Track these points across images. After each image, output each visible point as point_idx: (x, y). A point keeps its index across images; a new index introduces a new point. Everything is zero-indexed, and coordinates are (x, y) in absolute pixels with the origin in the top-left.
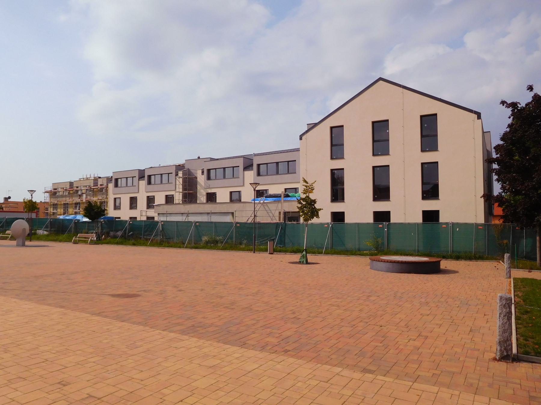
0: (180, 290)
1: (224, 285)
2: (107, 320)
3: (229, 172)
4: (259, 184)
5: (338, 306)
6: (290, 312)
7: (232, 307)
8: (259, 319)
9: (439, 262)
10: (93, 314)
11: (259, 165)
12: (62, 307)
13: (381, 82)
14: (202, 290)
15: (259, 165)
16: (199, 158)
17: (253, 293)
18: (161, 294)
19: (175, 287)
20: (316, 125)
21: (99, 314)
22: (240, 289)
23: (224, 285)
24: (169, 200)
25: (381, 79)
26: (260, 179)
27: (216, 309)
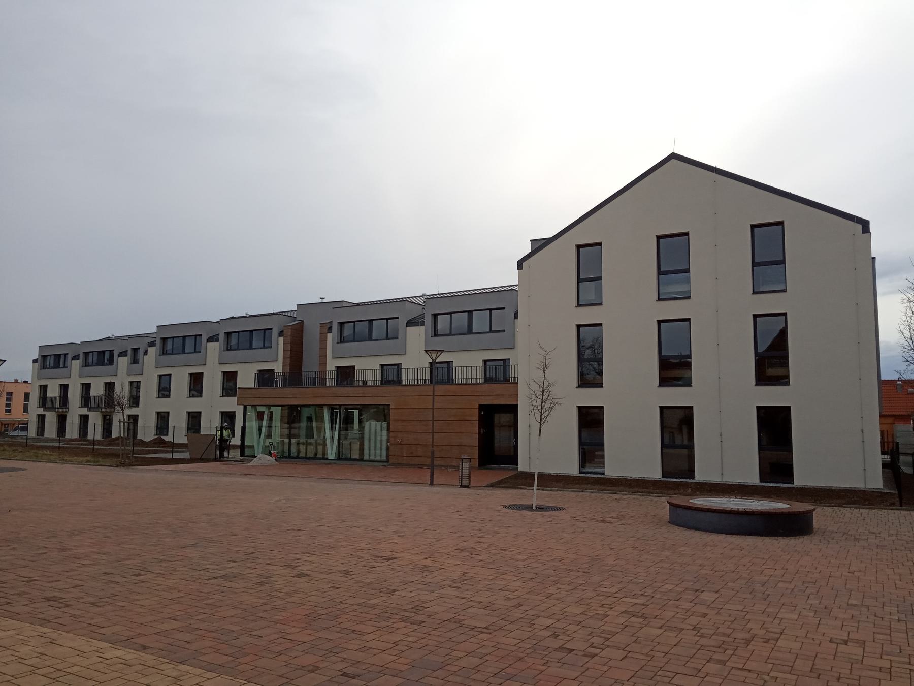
0: (301, 575)
1: (389, 559)
2: (149, 659)
3: (189, 344)
4: (442, 351)
5: (643, 617)
6: (547, 633)
7: (419, 618)
8: (484, 651)
9: (811, 512)
10: (115, 642)
11: (435, 316)
12: (45, 622)
13: (673, 161)
14: (347, 573)
15: (435, 316)
16: (16, 381)
17: (454, 581)
18: (262, 584)
19: (289, 566)
20: (548, 241)
21: (127, 642)
22: (425, 568)
23: (389, 559)
24: (265, 378)
25: (673, 156)
26: (438, 343)
27: (383, 624)
